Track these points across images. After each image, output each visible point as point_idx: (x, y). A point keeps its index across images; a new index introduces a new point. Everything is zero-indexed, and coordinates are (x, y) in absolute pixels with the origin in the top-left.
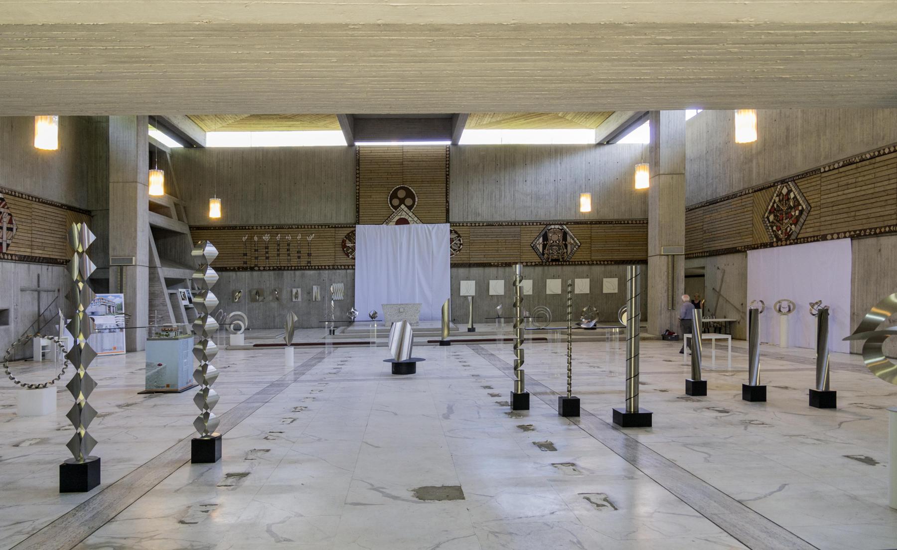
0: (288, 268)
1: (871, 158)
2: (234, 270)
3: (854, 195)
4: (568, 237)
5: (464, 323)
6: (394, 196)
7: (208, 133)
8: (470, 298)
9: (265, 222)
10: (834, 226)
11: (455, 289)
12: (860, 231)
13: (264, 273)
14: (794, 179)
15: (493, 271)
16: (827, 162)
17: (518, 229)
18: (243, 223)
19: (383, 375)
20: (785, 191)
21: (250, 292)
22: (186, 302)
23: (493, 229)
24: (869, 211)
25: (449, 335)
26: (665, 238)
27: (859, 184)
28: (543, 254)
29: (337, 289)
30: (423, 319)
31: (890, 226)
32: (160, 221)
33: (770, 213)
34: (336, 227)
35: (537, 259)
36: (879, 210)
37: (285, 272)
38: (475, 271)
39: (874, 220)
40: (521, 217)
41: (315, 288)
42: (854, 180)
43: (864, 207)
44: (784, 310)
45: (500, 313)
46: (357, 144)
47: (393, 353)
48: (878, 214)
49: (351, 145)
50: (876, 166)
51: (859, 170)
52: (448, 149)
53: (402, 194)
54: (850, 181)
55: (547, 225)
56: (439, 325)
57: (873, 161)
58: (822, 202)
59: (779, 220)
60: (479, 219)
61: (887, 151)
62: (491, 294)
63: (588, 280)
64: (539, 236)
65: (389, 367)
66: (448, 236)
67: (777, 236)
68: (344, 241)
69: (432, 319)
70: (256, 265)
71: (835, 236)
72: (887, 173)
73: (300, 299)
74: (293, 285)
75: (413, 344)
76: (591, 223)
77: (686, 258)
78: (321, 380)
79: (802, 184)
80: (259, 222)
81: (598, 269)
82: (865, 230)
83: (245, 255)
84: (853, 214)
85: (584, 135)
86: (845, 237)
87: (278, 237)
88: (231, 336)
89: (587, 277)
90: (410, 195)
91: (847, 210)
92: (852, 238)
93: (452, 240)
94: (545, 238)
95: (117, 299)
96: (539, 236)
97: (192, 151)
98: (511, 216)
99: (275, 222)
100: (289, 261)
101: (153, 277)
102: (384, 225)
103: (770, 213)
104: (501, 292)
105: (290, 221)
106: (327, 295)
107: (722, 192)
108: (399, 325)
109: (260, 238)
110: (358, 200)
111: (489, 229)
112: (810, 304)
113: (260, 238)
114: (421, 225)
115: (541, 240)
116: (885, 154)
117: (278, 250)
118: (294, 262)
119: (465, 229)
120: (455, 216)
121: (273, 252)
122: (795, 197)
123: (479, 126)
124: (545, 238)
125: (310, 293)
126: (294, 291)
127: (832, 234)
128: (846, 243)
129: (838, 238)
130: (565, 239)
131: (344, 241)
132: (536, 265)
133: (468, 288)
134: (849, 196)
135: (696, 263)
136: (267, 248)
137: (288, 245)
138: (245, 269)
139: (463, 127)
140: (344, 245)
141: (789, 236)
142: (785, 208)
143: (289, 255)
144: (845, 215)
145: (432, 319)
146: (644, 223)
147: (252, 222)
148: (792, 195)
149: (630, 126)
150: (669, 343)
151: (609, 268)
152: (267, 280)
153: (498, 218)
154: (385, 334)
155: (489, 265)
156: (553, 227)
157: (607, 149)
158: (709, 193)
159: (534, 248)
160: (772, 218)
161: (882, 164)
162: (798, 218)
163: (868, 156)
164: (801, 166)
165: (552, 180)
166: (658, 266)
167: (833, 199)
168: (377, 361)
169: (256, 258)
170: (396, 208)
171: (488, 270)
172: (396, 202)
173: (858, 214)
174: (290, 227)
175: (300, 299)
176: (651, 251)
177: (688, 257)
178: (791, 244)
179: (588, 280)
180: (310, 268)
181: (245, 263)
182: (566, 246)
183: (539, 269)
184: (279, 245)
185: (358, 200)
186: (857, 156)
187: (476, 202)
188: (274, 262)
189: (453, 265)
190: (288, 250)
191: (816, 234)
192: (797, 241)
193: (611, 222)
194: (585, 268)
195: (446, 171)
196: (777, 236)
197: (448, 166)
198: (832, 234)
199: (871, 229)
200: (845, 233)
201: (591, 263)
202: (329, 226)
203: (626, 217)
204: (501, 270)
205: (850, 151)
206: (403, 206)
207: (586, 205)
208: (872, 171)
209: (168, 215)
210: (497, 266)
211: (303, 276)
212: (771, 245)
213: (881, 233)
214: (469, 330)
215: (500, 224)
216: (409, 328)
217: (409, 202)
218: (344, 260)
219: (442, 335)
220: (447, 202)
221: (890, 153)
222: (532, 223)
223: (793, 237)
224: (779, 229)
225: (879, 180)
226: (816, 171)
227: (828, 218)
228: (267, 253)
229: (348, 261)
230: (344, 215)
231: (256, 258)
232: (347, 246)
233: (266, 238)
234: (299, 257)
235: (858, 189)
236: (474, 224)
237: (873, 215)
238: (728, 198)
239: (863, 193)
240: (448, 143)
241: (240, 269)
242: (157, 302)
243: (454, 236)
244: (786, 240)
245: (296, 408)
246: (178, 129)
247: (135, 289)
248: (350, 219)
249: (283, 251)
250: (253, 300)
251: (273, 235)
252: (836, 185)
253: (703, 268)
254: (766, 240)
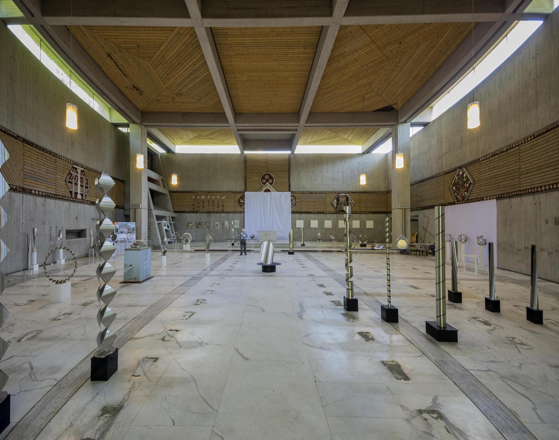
0: (214, 212)
1: (506, 151)
2: (188, 212)
3: (498, 173)
5: (298, 243)
6: (263, 178)
7: (177, 146)
8: (302, 229)
9: (202, 189)
10: (487, 192)
11: (294, 225)
12: (501, 194)
13: (203, 214)
14: (465, 166)
15: (312, 215)
16: (483, 155)
17: (324, 195)
18: (193, 190)
19: (256, 272)
20: (461, 173)
21: (196, 223)
22: (166, 228)
23: (312, 195)
24: (506, 183)
25: (293, 247)
26: (400, 200)
27: (501, 167)
29: (236, 223)
30: (278, 239)
31: (516, 192)
32: (154, 187)
33: (453, 186)
34: (235, 192)
35: (334, 210)
36: (510, 182)
37: (212, 214)
38: (303, 215)
39: (508, 188)
40: (326, 189)
41: (226, 222)
42: (497, 165)
43: (503, 180)
44: (463, 241)
45: (320, 237)
46: (245, 152)
47: (262, 260)
48: (510, 185)
49: (242, 153)
50: (509, 155)
51: (501, 158)
52: (289, 155)
53: (267, 177)
54: (496, 165)
56: (288, 242)
57: (507, 152)
58: (481, 178)
59: (458, 189)
60: (305, 190)
61: (514, 146)
62: (311, 227)
63: (359, 221)
64: (335, 199)
65: (260, 268)
66: (290, 198)
67: (457, 199)
68: (239, 200)
69: (283, 239)
71: (488, 198)
72: (514, 159)
73: (219, 227)
74: (216, 220)
75: (274, 252)
76: (360, 193)
77: (411, 211)
78: (221, 275)
79: (470, 168)
80: (200, 190)
81: (363, 216)
82: (504, 194)
84: (497, 185)
85: (356, 149)
86: (493, 198)
87: (209, 197)
88: (184, 245)
89: (358, 220)
90: (271, 177)
91: (494, 182)
92: (497, 199)
93: (292, 200)
94: (338, 200)
95: (132, 225)
96: (335, 199)
97: (170, 154)
98: (321, 189)
99: (207, 190)
100: (214, 208)
101: (150, 215)
102: (259, 192)
103: (453, 186)
104: (317, 226)
105: (214, 189)
106: (231, 226)
107: (427, 175)
108: (266, 243)
109: (200, 197)
110: (246, 180)
111: (310, 195)
112: (478, 238)
113: (200, 197)
114: (276, 192)
115: (336, 201)
116: (513, 148)
118: (216, 209)
119: (298, 195)
120: (293, 189)
121: (206, 204)
122: (467, 176)
123: (305, 144)
124: (338, 200)
125: (223, 224)
126: (216, 223)
127: (487, 197)
128: (493, 203)
129: (490, 199)
130: (347, 200)
131: (239, 200)
132: (333, 213)
133: (300, 224)
134: (495, 174)
135: (415, 213)
136: (203, 202)
138: (193, 212)
139: (297, 145)
140: (239, 202)
141: (463, 198)
142: (461, 183)
144: (493, 186)
145: (283, 239)
146: (389, 192)
147: (196, 189)
148: (465, 175)
149: (380, 142)
150: (406, 256)
151: (369, 215)
152: (203, 217)
153: (314, 190)
154: (259, 246)
155: (310, 213)
157: (367, 155)
158: (420, 176)
159: (332, 205)
160: (454, 188)
161: (511, 154)
162: (468, 188)
163: (505, 150)
164: (469, 159)
165: (341, 171)
166: (397, 214)
167: (486, 177)
168: (253, 262)
169: (199, 207)
170: (264, 184)
171: (310, 215)
172: (264, 181)
173: (500, 184)
174: (214, 192)
175: (219, 227)
176: (393, 205)
177: (412, 210)
178: (465, 203)
179: (359, 221)
180: (224, 212)
181: (194, 209)
183: (335, 215)
185: (246, 180)
186: (499, 150)
187: (304, 182)
188: (206, 209)
189: (293, 213)
191: (478, 197)
192: (469, 201)
193: (369, 192)
194: (358, 215)
195: (288, 167)
196: (457, 199)
197: (289, 164)
198: (487, 197)
199: (507, 193)
200: (493, 196)
201: (360, 213)
202: (232, 192)
203: (377, 190)
204: (316, 215)
205: (494, 148)
206: (267, 183)
207: (363, 180)
208: (507, 159)
209: (159, 185)
210: (314, 213)
211: (220, 216)
212: (454, 204)
213: (512, 196)
214: (302, 245)
215: (316, 193)
216: (271, 244)
217: (270, 181)
218: (239, 209)
219: (289, 247)
220: (289, 181)
221: (516, 146)
222: (331, 192)
223: (466, 199)
224: (458, 194)
225: (510, 163)
226: (478, 161)
227: (485, 187)
229: (241, 210)
230: (239, 187)
231: (199, 207)
232: (241, 202)
233: (203, 197)
235: (500, 170)
236: (302, 193)
237: (508, 185)
238: (430, 178)
239: (502, 172)
240: (289, 152)
241: (191, 212)
242: (152, 227)
243: (293, 198)
244: (462, 201)
245: (198, 301)
246: (164, 144)
247: (141, 220)
248: (242, 188)
249: (211, 204)
250: (197, 227)
251: (206, 196)
252: (488, 168)
253: (417, 216)
254: (452, 201)
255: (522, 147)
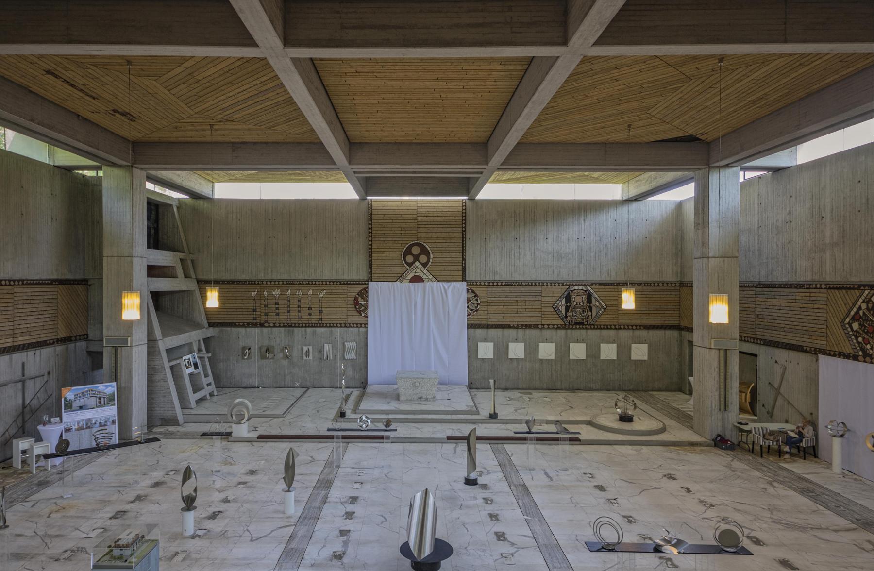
4: (593, 300)
28: (566, 317)
55: (570, 286)
70: (266, 322)
83: (255, 310)
87: (289, 293)
94: (568, 299)
109: (270, 293)
113: (270, 293)
117: (289, 306)
118: (305, 319)
121: (283, 309)
124: (568, 299)
130: (589, 300)
136: (277, 304)
137: (299, 301)
143: (299, 311)
156: (576, 288)
159: (556, 309)
174: (301, 282)
182: (591, 308)
184: (289, 301)
190: (299, 306)
212: (856, 358)
228: (277, 309)
233: (276, 293)
234: (310, 314)
249: (294, 307)
251: (283, 291)
255: (343, 321)
